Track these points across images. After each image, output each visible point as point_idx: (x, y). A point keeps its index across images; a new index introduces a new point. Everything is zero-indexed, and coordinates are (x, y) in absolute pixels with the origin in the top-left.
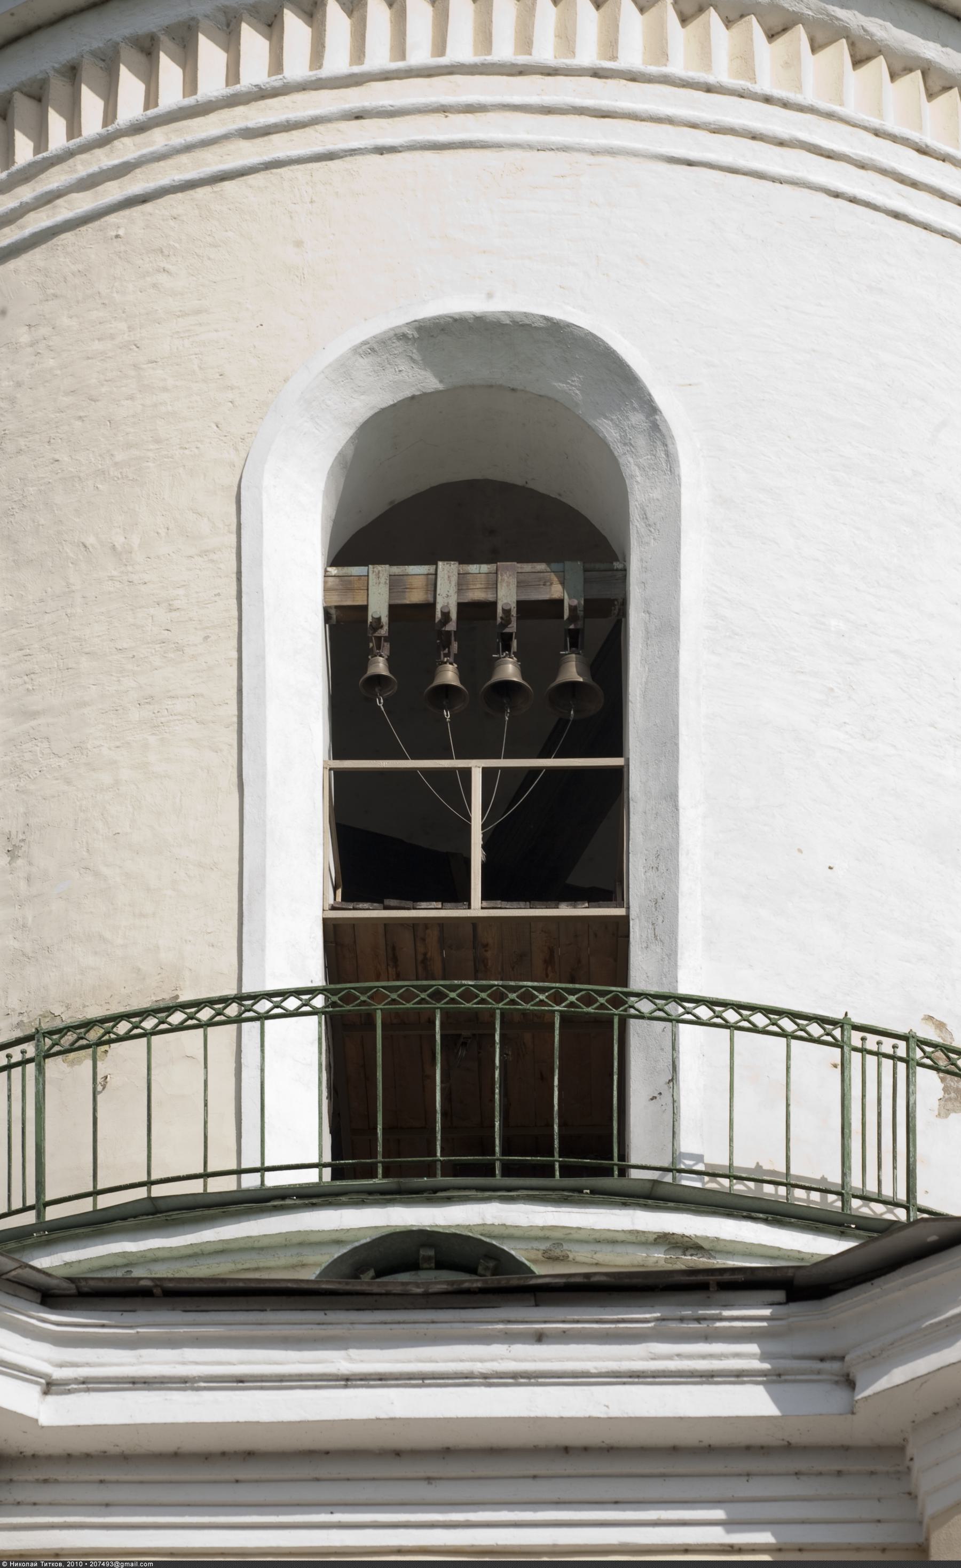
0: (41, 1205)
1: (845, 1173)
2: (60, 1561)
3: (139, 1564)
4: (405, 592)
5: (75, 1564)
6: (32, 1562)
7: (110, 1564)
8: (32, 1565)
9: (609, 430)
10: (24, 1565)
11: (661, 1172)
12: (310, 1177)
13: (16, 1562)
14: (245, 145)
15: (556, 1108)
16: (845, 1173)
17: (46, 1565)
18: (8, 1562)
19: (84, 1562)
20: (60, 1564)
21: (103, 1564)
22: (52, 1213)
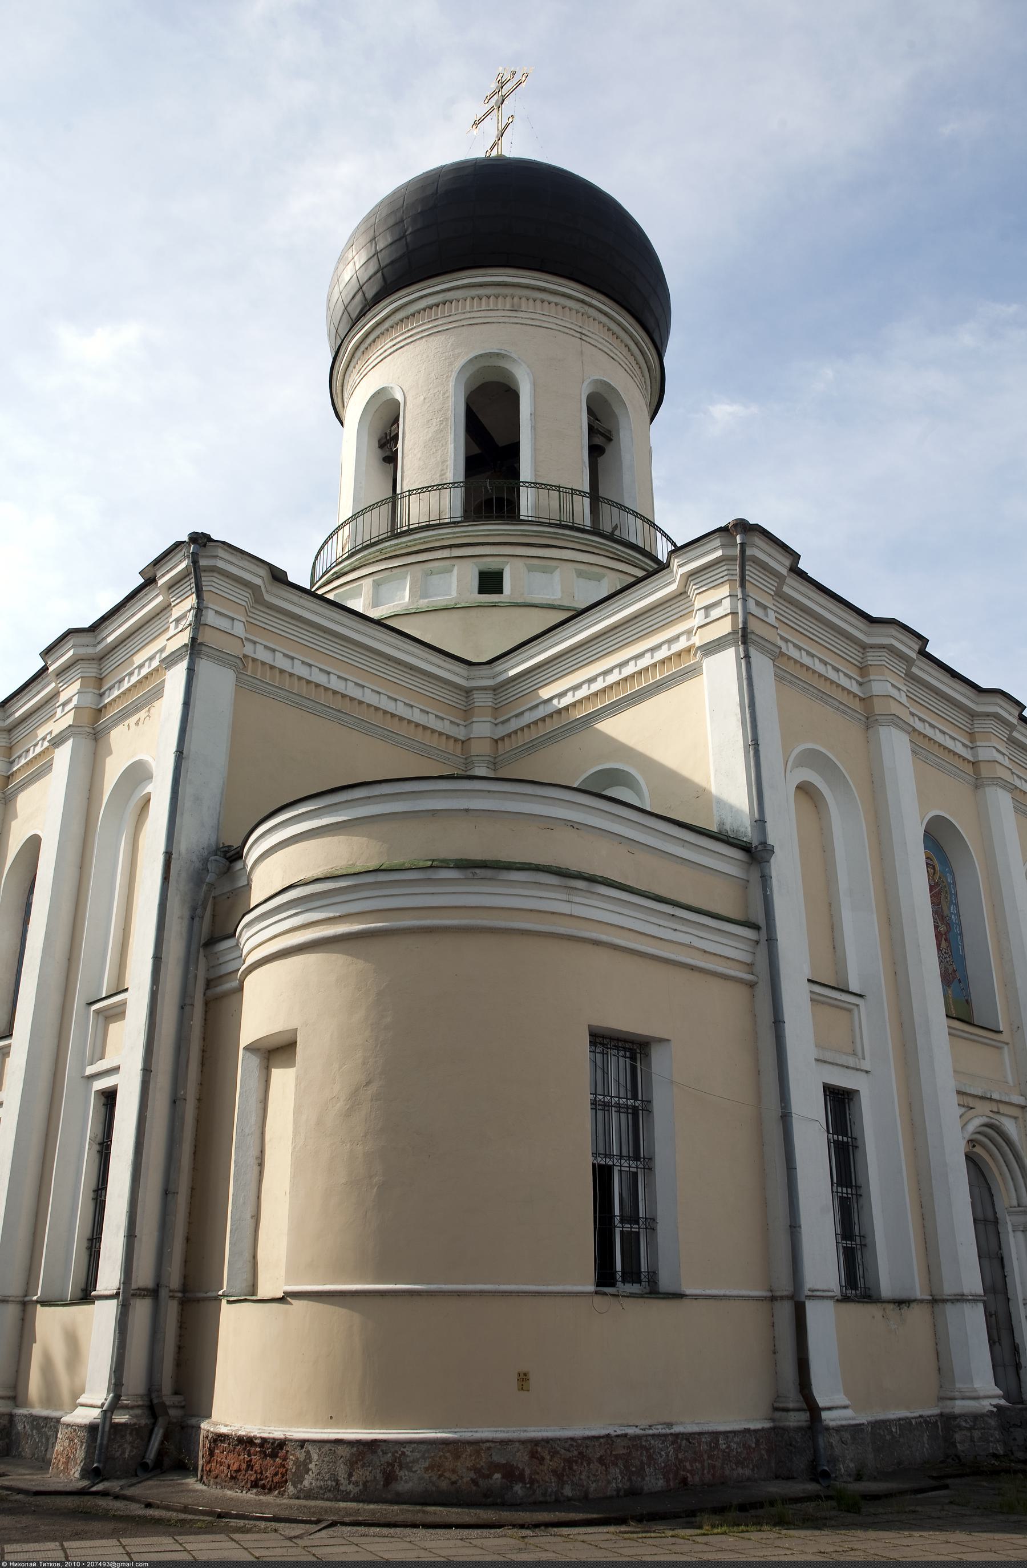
0: (409, 525)
1: (560, 517)
2: (58, 1562)
3: (134, 1564)
4: (1007, 739)
5: (73, 1564)
6: (31, 1562)
7: (107, 1564)
8: (31, 1565)
9: (507, 366)
10: (23, 1565)
11: (603, 793)
12: (459, 519)
13: (15, 1562)
14: (469, 314)
15: (619, 1267)
16: (560, 517)
17: (44, 1565)
18: (8, 1562)
19: (81, 1562)
20: (58, 1565)
21: (100, 1564)
22: (411, 527)
